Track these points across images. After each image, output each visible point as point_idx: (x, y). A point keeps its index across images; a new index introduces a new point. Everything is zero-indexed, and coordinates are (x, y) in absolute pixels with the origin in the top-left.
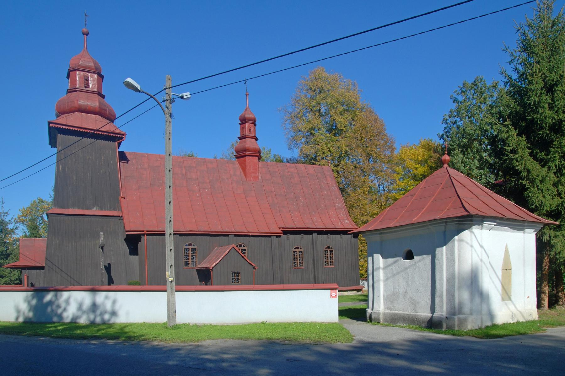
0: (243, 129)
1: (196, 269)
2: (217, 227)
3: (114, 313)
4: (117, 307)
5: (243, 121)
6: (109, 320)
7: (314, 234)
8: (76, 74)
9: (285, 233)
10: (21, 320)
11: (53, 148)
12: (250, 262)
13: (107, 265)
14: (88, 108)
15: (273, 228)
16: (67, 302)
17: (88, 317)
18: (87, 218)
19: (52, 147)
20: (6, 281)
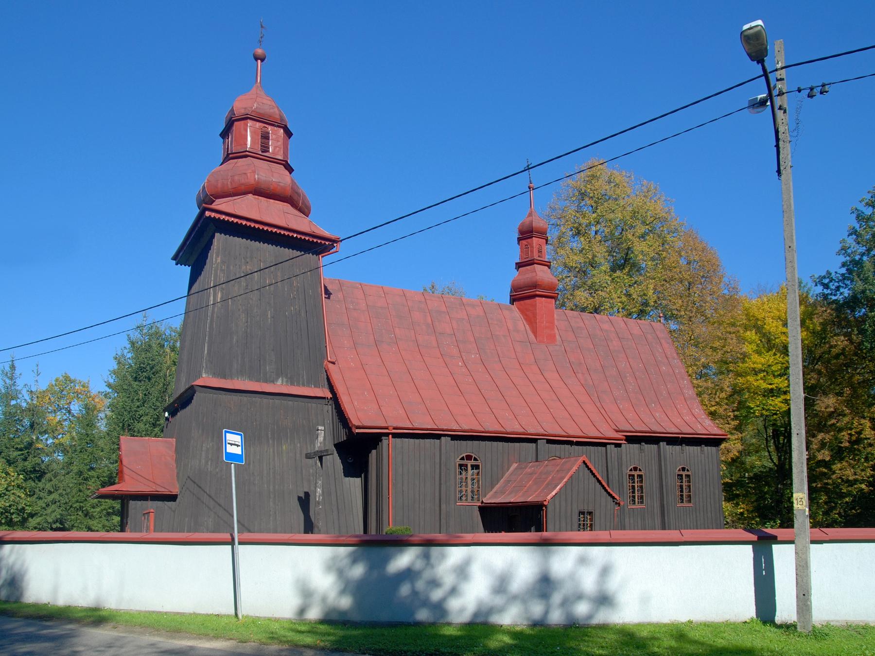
0: (525, 250)
1: (480, 507)
2: (512, 427)
3: (604, 600)
4: (613, 584)
5: (526, 234)
6: (590, 617)
7: (661, 443)
8: (247, 125)
9: (631, 440)
10: (314, 614)
11: (179, 265)
12: (611, 493)
13: (302, 495)
14: (272, 187)
15: (604, 429)
16: (462, 571)
17: (526, 610)
18: (266, 400)
19: (177, 264)
20: (39, 524)
